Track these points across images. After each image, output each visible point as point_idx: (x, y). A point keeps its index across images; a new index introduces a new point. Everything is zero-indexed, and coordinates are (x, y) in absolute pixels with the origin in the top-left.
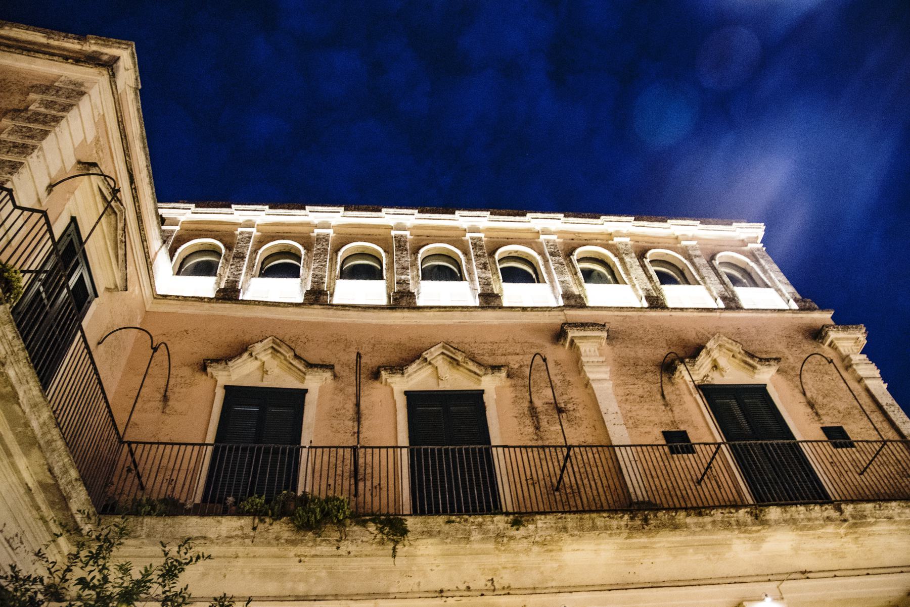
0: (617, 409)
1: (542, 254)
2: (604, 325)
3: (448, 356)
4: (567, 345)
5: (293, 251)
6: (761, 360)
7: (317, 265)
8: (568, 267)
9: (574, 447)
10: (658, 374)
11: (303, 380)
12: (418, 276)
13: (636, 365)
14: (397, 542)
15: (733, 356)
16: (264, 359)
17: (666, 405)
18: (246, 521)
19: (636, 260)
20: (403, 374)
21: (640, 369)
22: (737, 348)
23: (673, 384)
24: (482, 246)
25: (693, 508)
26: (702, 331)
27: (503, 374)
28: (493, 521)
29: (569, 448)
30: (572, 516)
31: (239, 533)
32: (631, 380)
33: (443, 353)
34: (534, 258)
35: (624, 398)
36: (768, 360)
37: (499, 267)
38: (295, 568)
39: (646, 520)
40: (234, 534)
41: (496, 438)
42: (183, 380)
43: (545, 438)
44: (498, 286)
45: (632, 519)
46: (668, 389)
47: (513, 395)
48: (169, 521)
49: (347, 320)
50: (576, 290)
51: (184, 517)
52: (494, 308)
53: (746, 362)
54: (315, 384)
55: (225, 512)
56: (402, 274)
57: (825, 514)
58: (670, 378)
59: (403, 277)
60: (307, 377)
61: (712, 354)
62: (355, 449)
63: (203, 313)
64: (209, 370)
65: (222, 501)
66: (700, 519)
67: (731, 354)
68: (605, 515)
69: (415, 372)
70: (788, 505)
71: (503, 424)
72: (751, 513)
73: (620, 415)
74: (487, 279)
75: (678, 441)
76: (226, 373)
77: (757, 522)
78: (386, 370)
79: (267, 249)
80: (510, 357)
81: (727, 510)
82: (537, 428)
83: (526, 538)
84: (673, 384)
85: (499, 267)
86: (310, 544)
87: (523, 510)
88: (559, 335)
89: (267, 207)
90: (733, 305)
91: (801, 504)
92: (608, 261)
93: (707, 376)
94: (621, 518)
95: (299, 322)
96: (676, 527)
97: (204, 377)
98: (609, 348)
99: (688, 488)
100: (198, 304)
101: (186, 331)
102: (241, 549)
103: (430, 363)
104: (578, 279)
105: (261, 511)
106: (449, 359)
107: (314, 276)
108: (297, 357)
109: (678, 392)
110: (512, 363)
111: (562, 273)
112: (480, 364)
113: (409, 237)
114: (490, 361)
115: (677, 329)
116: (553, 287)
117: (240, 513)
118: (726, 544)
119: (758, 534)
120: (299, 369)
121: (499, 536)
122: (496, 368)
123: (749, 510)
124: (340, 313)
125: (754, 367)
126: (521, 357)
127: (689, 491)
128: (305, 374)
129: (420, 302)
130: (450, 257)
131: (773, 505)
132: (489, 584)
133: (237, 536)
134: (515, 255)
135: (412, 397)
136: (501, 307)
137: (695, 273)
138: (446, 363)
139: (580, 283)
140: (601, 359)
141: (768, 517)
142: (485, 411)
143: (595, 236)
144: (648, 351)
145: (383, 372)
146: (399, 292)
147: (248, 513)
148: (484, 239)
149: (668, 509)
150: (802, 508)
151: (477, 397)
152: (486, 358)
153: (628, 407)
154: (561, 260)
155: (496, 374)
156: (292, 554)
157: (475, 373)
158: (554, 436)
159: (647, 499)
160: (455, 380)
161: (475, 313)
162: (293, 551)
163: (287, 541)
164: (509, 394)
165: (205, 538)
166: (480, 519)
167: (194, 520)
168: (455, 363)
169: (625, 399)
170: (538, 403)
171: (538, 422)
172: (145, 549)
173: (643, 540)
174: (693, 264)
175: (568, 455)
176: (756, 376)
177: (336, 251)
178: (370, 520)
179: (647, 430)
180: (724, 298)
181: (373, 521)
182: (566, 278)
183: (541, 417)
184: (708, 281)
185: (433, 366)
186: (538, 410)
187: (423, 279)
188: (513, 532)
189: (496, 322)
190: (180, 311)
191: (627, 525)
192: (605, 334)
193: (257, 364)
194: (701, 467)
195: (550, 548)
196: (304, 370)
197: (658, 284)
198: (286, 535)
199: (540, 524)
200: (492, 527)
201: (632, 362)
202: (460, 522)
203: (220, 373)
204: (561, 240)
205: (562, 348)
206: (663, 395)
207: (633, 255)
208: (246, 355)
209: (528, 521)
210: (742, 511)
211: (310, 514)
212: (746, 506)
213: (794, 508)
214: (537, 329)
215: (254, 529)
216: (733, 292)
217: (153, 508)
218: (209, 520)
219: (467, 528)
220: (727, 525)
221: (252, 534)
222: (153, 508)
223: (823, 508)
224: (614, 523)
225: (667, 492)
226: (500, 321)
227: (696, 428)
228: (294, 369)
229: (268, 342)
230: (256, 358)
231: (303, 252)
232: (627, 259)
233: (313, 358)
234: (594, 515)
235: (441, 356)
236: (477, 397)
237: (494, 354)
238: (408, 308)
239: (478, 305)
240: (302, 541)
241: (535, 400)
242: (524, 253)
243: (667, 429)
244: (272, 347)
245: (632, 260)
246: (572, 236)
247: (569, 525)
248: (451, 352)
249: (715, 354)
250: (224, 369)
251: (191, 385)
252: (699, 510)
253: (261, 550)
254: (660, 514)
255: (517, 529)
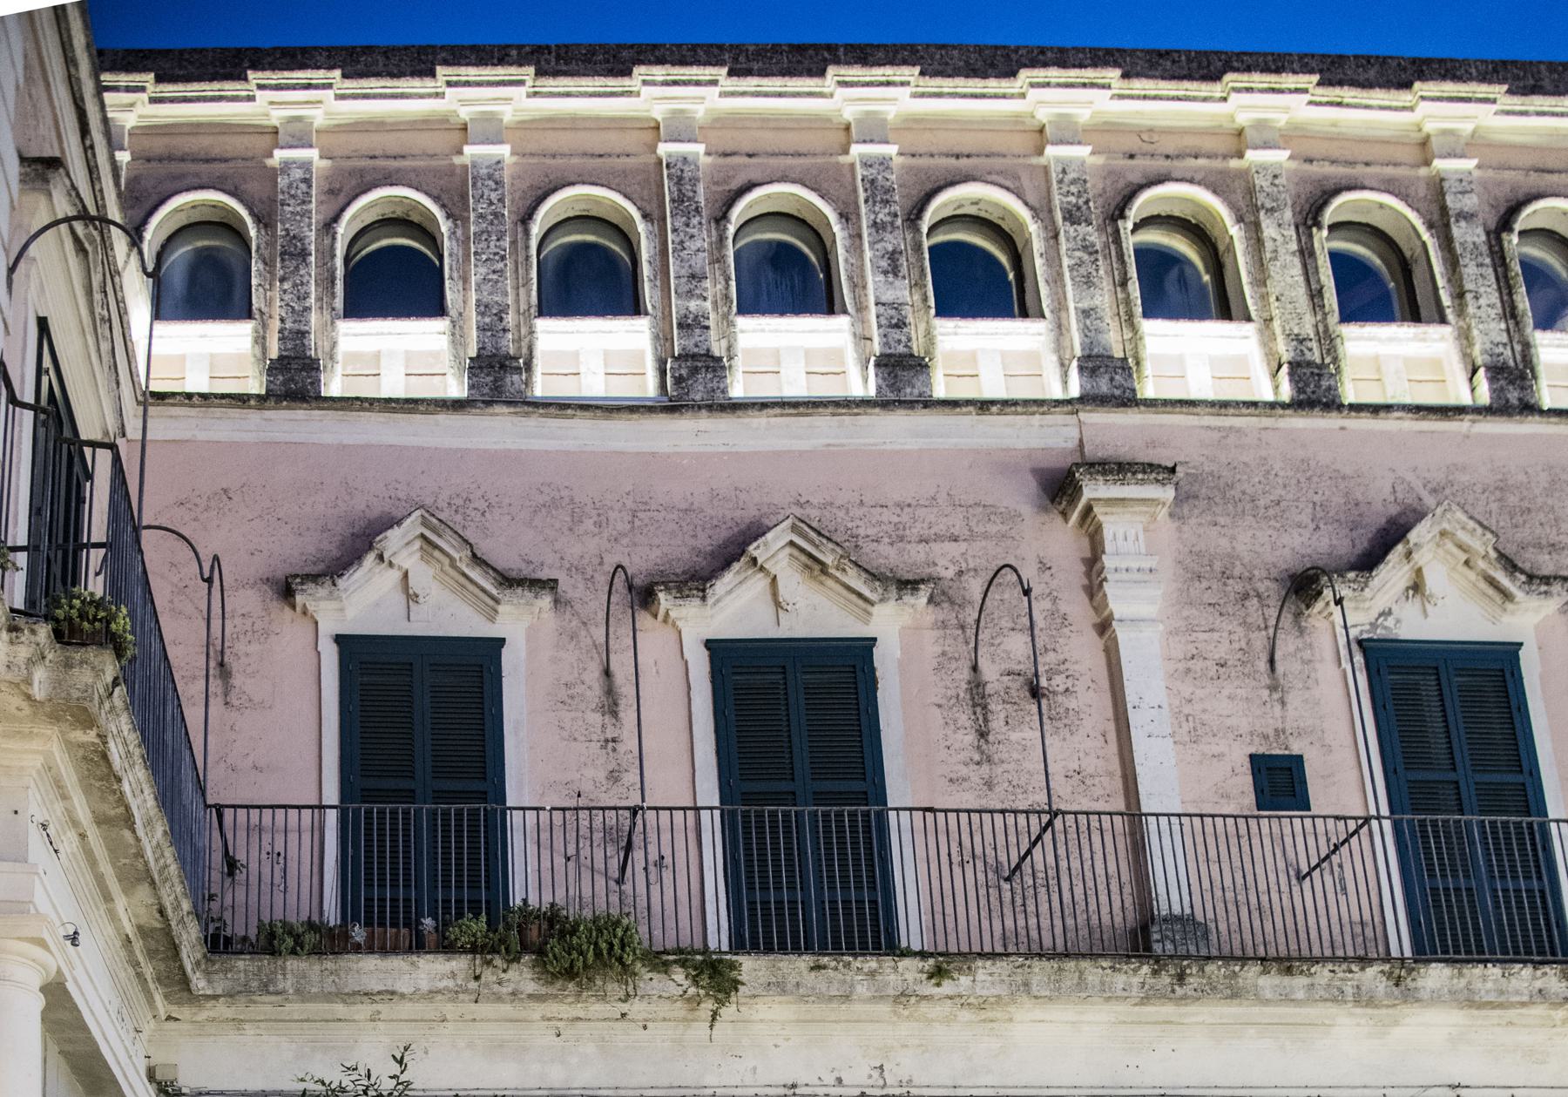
0: (1161, 696)
1: (1042, 211)
2: (1173, 470)
3: (802, 550)
4: (1075, 516)
5: (415, 218)
6: (1531, 577)
7: (483, 270)
8: (1108, 256)
9: (1064, 813)
10: (1274, 602)
11: (492, 615)
12: (727, 297)
13: (1225, 575)
14: (721, 1003)
15: (1467, 563)
16: (406, 566)
17: (1273, 688)
18: (460, 964)
19: (1292, 232)
20: (704, 598)
21: (1236, 586)
22: (1480, 544)
23: (1301, 631)
24: (890, 190)
25: (1278, 959)
26: (1410, 477)
27: (922, 598)
28: (896, 969)
29: (1055, 814)
30: (1045, 963)
31: (450, 984)
32: (1205, 618)
33: (792, 543)
34: (1022, 226)
35: (1181, 666)
36: (1547, 580)
37: (926, 244)
38: (542, 1037)
39: (1181, 978)
40: (441, 985)
41: (901, 787)
42: (249, 622)
43: (996, 758)
44: (922, 327)
45: (1155, 973)
46: (1287, 645)
47: (939, 650)
48: (329, 963)
49: (570, 445)
50: (1114, 341)
51: (353, 957)
52: (910, 404)
53: (1492, 582)
54: (518, 624)
55: (418, 946)
56: (690, 294)
57: (1538, 984)
58: (1298, 615)
59: (693, 305)
60: (500, 608)
61: (1415, 556)
62: (634, 811)
63: (249, 437)
64: (299, 599)
65: (413, 924)
66: (1287, 980)
67: (1464, 557)
68: (1105, 964)
69: (730, 592)
70: (1468, 961)
71: (919, 753)
72: (1389, 975)
73: (1166, 710)
74: (896, 306)
75: (1280, 782)
76: (333, 605)
77: (1396, 991)
78: (668, 589)
79: (354, 217)
80: (936, 547)
81: (1344, 966)
82: (983, 735)
83: (951, 998)
84: (1301, 631)
85: (926, 244)
86: (570, 1000)
87: (953, 949)
88: (1059, 487)
89: (337, 73)
90: (1513, 396)
91: (1495, 962)
92: (1215, 233)
93: (1387, 613)
94: (1135, 971)
95: (463, 454)
96: (1235, 995)
97: (287, 609)
98: (1172, 525)
99: (1274, 888)
100: (235, 413)
101: (225, 491)
102: (450, 1006)
103: (762, 569)
104: (1128, 301)
105: (484, 946)
106: (803, 558)
107: (483, 308)
108: (477, 560)
109: (1307, 654)
110: (942, 562)
111: (1088, 282)
112: (873, 576)
113: (704, 161)
114: (887, 556)
115: (1348, 471)
116: (1060, 328)
117: (447, 947)
118: (1324, 1024)
119: (1390, 1011)
120: (484, 590)
121: (902, 997)
122: (908, 585)
123: (1387, 967)
124: (554, 424)
125: (1507, 596)
126: (963, 546)
127: (1275, 896)
128: (497, 601)
129: (738, 388)
130: (803, 222)
131: (1440, 961)
132: (876, 1074)
133: (446, 988)
134: (972, 210)
135: (718, 650)
136: (929, 404)
137: (1438, 268)
138: (796, 564)
139: (1130, 315)
140: (1147, 563)
141: (1420, 983)
142: (876, 689)
143: (1190, 142)
144: (1263, 536)
145: (661, 596)
146: (685, 357)
147: (463, 951)
148: (898, 161)
149: (1229, 958)
150: (1494, 971)
151: (855, 659)
152: (884, 548)
153: (1186, 689)
154: (1096, 239)
155: (908, 598)
156: (537, 1016)
157: (860, 595)
158: (1015, 756)
159: (1188, 911)
160: (815, 612)
161: (864, 420)
162: (538, 1010)
163: (530, 996)
164: (931, 645)
165: (393, 993)
166: (872, 963)
167: (370, 963)
168: (817, 567)
169: (1187, 667)
170: (989, 671)
171: (986, 720)
172: (288, 1007)
173: (1167, 1010)
174: (1447, 243)
175: (1050, 823)
176: (1506, 619)
177: (526, 218)
178: (675, 962)
179: (1216, 750)
180: (1497, 371)
181: (683, 964)
182: (1097, 301)
183: (992, 707)
184: (1471, 310)
185: (768, 573)
186: (989, 689)
187: (742, 311)
188: (929, 988)
189: (912, 444)
190: (202, 436)
191: (1143, 984)
192: (1168, 493)
193: (395, 575)
194: (1313, 851)
195: (990, 1014)
196: (494, 592)
197: (1334, 318)
198: (531, 987)
199: (981, 975)
200: (892, 977)
201: (1218, 566)
202: (836, 969)
203: (323, 604)
204: (1099, 160)
205: (1059, 519)
206: (1272, 661)
207: (1288, 215)
208: (370, 559)
209: (960, 970)
210: (1372, 971)
211: (575, 955)
212: (1388, 958)
213: (1479, 970)
214: (1002, 464)
215: (477, 978)
216: (1527, 346)
217: (298, 939)
218: (397, 963)
219: (848, 978)
220: (1338, 998)
221: (473, 985)
222: (298, 939)
223: (1539, 973)
224: (1120, 980)
225: (1230, 895)
226: (921, 443)
227: (1328, 749)
228: (471, 587)
229: (412, 526)
230: (391, 564)
231: (445, 226)
232: (1269, 230)
233: (507, 559)
234: (1085, 964)
235: (788, 550)
236: (855, 659)
237: (901, 539)
238: (710, 408)
239: (872, 392)
240: (556, 996)
241: (983, 663)
242: (997, 205)
243: (1262, 750)
244: (423, 536)
245: (1279, 232)
246: (1132, 144)
247: (1035, 980)
248: (811, 542)
249: (1421, 558)
250: (330, 597)
251: (266, 633)
252: (1287, 964)
253: (485, 1009)
254: (1211, 968)
255: (938, 985)
